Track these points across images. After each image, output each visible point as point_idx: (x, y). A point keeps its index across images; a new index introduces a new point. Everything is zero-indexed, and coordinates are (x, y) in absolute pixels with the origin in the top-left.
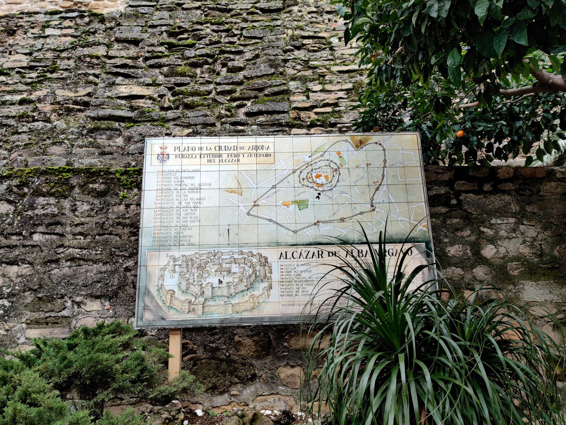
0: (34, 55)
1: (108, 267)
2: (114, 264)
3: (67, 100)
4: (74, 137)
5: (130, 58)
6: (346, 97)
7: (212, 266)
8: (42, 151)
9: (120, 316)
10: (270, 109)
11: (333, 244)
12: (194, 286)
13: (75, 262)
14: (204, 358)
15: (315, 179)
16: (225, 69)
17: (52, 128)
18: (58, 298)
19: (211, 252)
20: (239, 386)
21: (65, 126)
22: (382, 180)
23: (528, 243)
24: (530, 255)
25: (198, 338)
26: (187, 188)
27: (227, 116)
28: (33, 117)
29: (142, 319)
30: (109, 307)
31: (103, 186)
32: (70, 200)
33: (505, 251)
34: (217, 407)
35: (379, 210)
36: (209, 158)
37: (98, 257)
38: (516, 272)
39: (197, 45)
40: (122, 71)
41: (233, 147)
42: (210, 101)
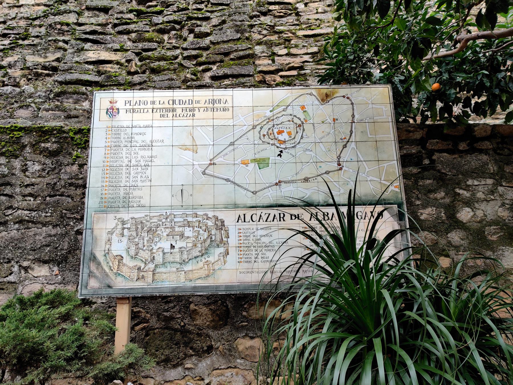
0: (8, 24)
1: (59, 230)
2: (64, 226)
3: (37, 65)
4: (41, 100)
5: (99, 25)
6: (311, 60)
7: (163, 230)
8: (9, 114)
9: (68, 283)
10: (235, 73)
11: (296, 206)
12: (144, 251)
13: (23, 225)
14: (157, 328)
15: (276, 136)
16: (192, 35)
17: (21, 92)
18: (5, 263)
19: (162, 215)
20: (194, 358)
21: (33, 90)
22: (350, 136)
23: (508, 206)
24: (510, 218)
25: (152, 306)
26: (138, 145)
27: (193, 80)
28: (4, 82)
29: (86, 287)
30: (57, 272)
31: (55, 146)
32: (21, 160)
33: (482, 215)
34: (169, 381)
35: (347, 169)
36: (161, 113)
37: (48, 219)
38: (495, 237)
39: (165, 12)
40: (91, 37)
41: (187, 101)
42: (177, 66)
